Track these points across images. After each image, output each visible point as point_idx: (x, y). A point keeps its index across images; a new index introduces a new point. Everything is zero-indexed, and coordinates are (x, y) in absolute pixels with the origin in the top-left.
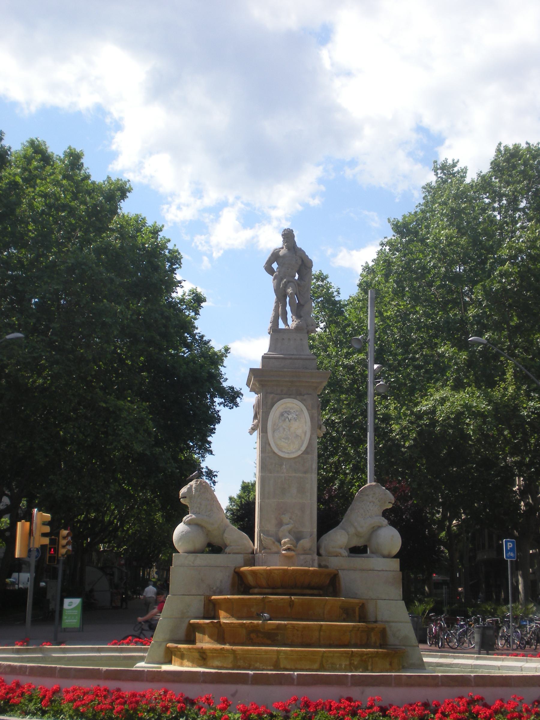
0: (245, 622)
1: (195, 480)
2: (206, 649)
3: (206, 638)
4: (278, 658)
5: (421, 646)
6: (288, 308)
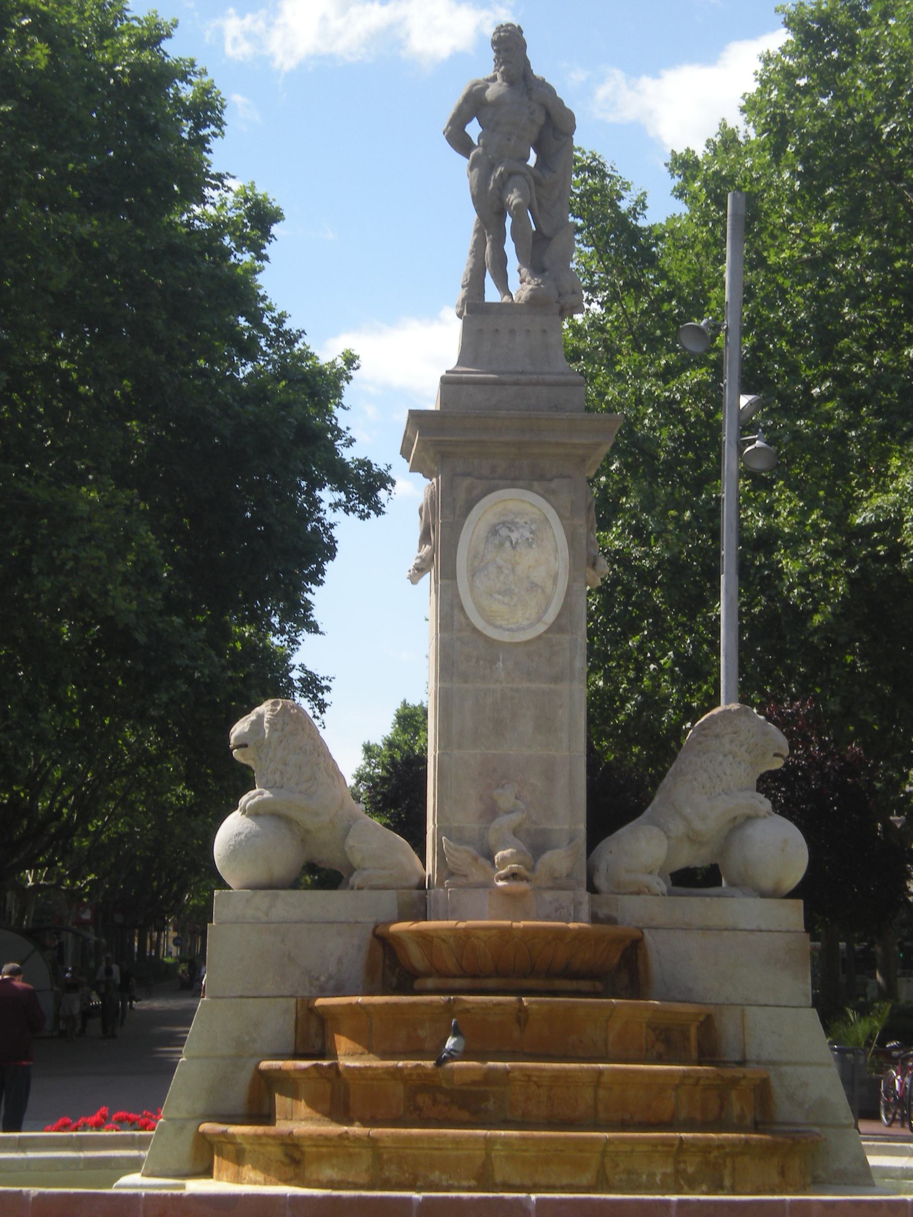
0: (400, 1064)
1: (270, 701)
2: (300, 1137)
3: (302, 1107)
4: (488, 1156)
5: (865, 1126)
6: (510, 247)
